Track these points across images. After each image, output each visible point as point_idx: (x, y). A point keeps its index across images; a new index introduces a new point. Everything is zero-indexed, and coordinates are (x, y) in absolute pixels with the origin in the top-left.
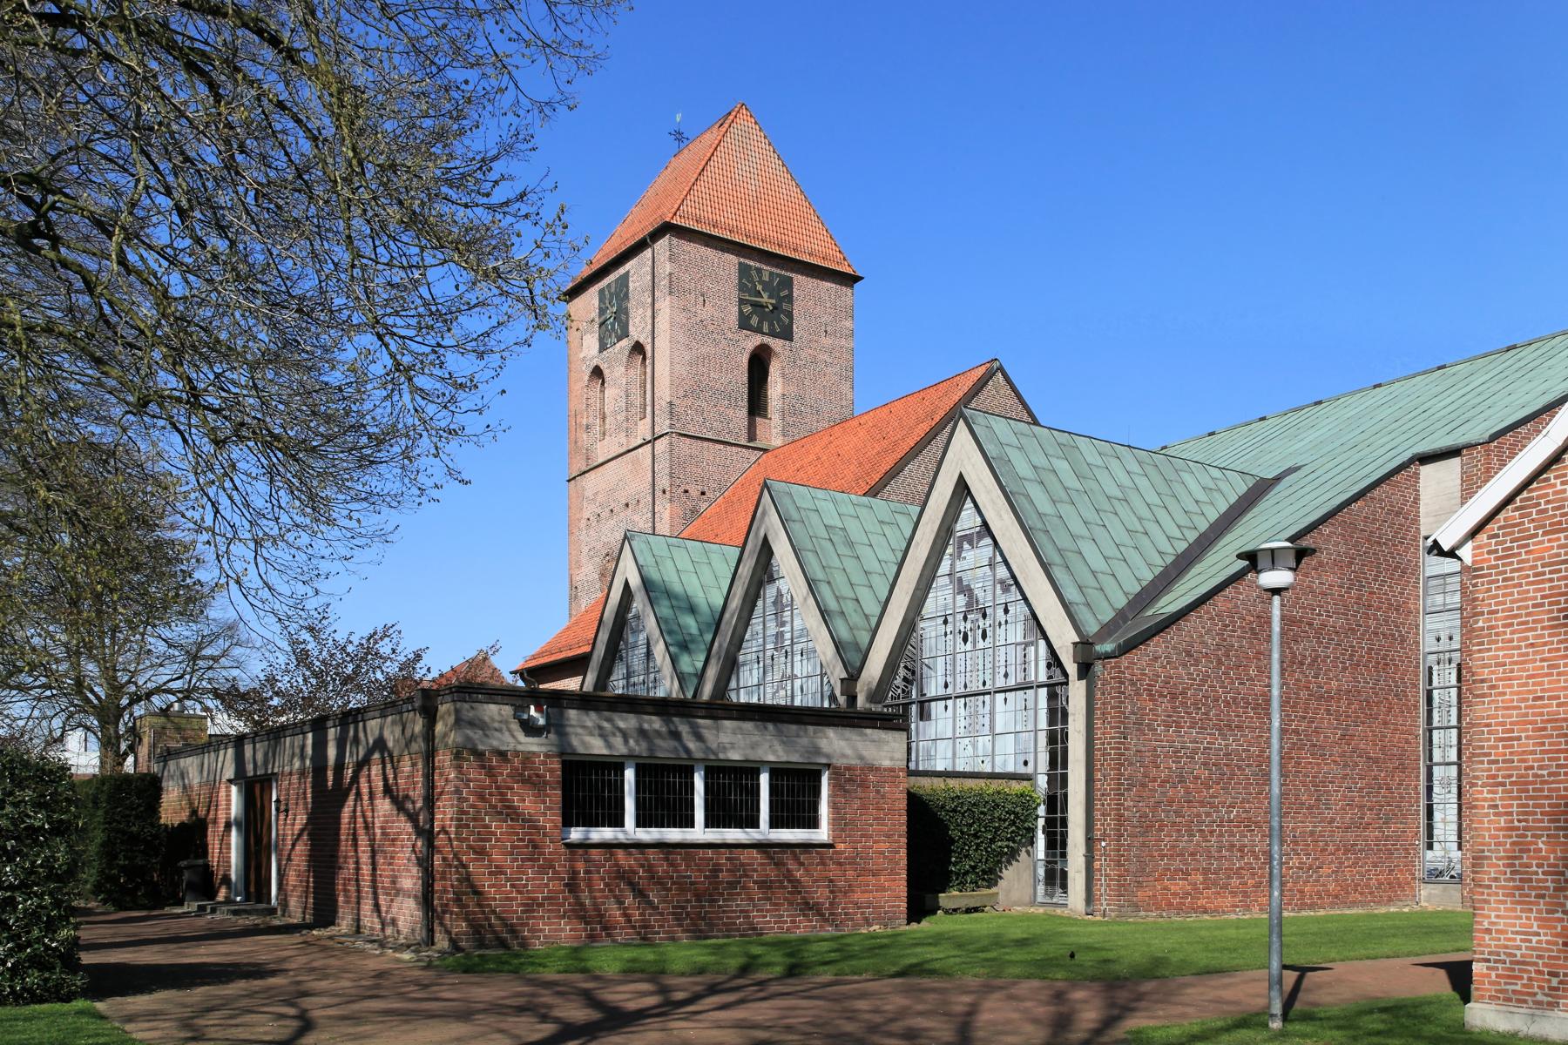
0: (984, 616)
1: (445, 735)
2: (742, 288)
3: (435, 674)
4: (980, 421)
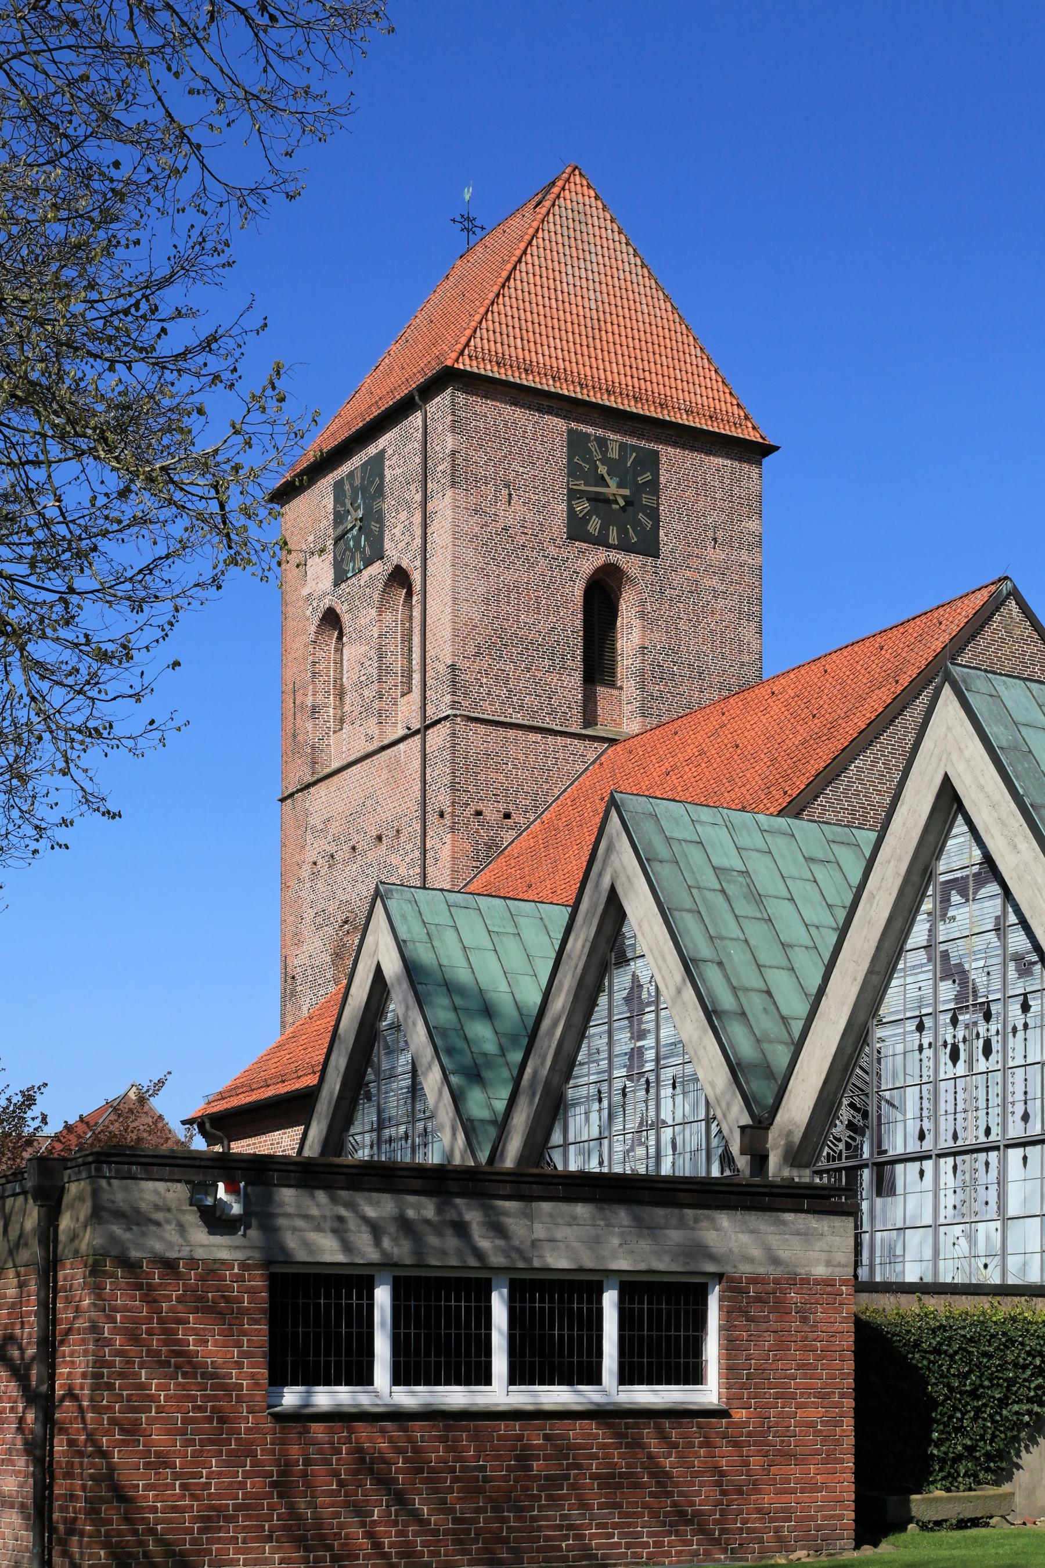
0: (988, 1017)
1: (74, 1237)
2: (573, 471)
3: (54, 1127)
4: (979, 685)
